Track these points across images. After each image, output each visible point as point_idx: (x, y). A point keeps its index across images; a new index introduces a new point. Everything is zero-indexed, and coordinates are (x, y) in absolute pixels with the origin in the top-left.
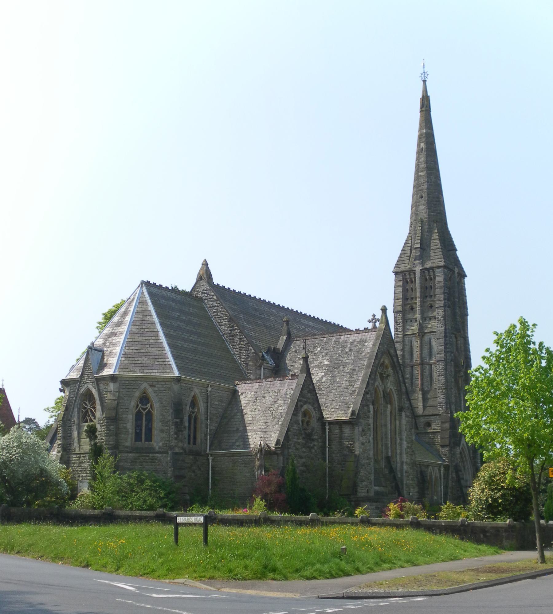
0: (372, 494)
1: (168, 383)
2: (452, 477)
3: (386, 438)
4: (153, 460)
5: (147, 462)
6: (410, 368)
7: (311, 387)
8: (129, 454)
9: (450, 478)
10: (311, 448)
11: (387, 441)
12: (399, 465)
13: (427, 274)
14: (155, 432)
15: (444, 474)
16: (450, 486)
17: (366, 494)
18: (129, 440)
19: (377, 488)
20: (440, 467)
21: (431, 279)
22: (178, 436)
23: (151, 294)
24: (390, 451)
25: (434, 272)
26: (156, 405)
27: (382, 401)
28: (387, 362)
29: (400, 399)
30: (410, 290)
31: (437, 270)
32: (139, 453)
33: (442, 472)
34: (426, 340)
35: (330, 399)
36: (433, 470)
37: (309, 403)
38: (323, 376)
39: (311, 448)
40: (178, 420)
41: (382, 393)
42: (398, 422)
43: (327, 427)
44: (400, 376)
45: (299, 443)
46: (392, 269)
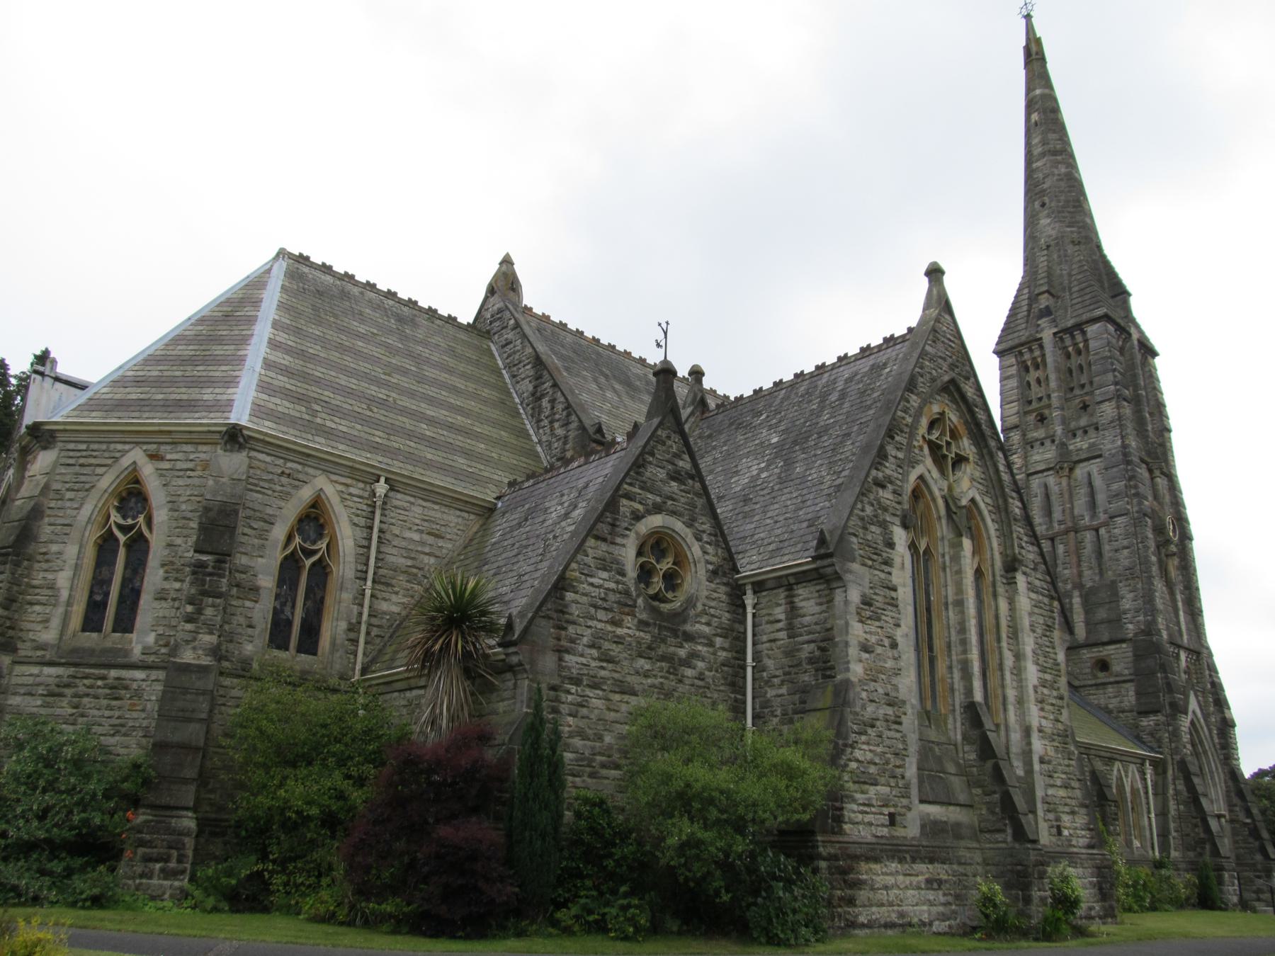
0: (911, 830)
1: (204, 448)
2: (1177, 792)
3: (964, 642)
4: (116, 689)
5: (96, 697)
6: (1049, 543)
7: (684, 464)
8: (48, 670)
9: (1171, 792)
10: (675, 665)
11: (965, 652)
12: (1016, 737)
13: (1068, 342)
14: (146, 600)
15: (1155, 786)
16: (1173, 812)
17: (884, 831)
18: (55, 623)
19: (934, 811)
20: (1143, 764)
21: (1079, 352)
22: (199, 611)
23: (291, 275)
24: (977, 684)
25: (1084, 333)
26: (161, 515)
27: (943, 529)
28: (953, 417)
29: (1006, 535)
30: (1033, 383)
31: (1092, 330)
32: (76, 665)
33: (1148, 776)
34: (1080, 478)
35: (768, 521)
36: (1126, 772)
37: (673, 513)
38: (761, 470)
39: (675, 665)
40: (204, 558)
41: (940, 502)
42: (1003, 605)
43: (749, 600)
44: (1002, 468)
45: (619, 641)
46: (993, 346)
